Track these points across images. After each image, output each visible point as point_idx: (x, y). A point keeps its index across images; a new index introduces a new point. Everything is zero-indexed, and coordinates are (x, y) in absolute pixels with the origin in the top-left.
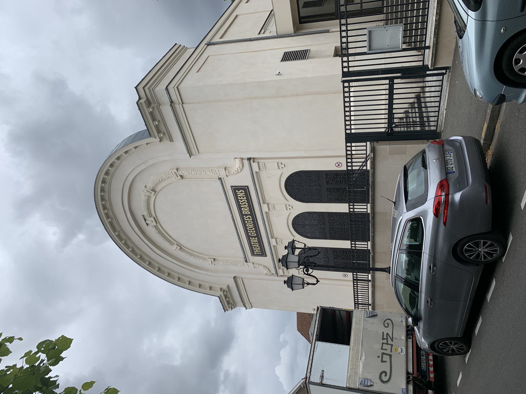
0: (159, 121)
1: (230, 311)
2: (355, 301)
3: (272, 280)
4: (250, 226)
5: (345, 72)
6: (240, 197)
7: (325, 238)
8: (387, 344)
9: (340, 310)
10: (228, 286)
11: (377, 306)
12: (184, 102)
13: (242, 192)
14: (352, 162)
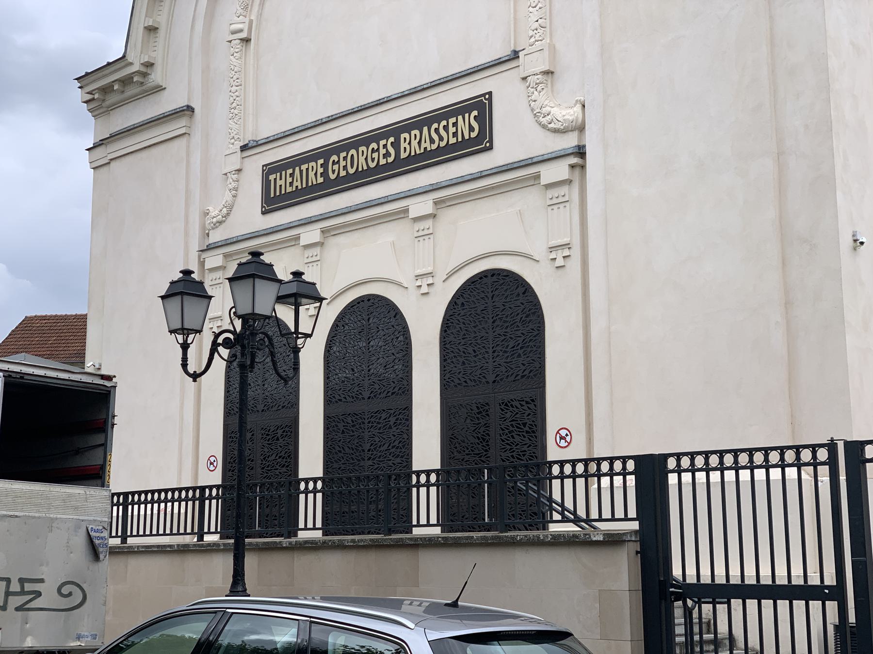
1: (77, 95)
2: (133, 494)
3: (187, 234)
4: (362, 159)
5: (863, 451)
6: (455, 124)
7: (329, 401)
8: (8, 594)
9: (105, 447)
10: (159, 89)
11: (120, 561)
13: (471, 129)
14: (574, 476)
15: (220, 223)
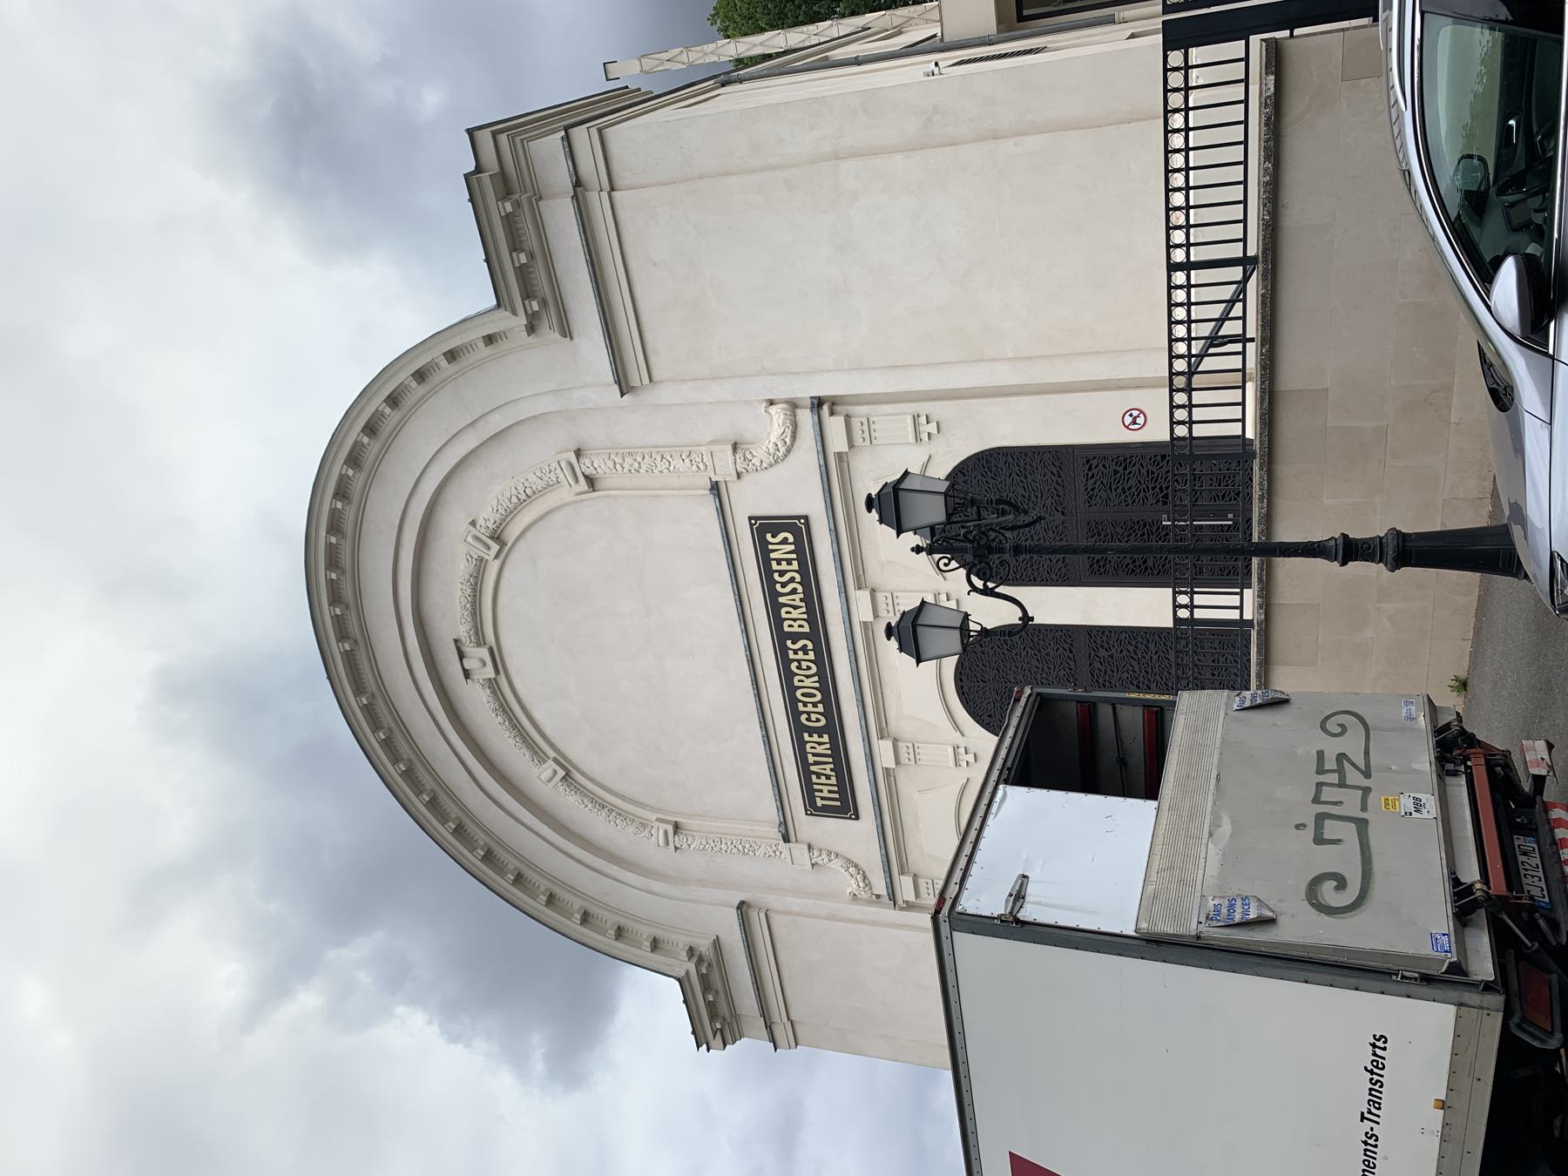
0: (531, 256)
3: (875, 924)
6: (779, 562)
8: (1342, 784)
10: (717, 943)
12: (618, 182)
13: (785, 541)
15: (865, 877)
